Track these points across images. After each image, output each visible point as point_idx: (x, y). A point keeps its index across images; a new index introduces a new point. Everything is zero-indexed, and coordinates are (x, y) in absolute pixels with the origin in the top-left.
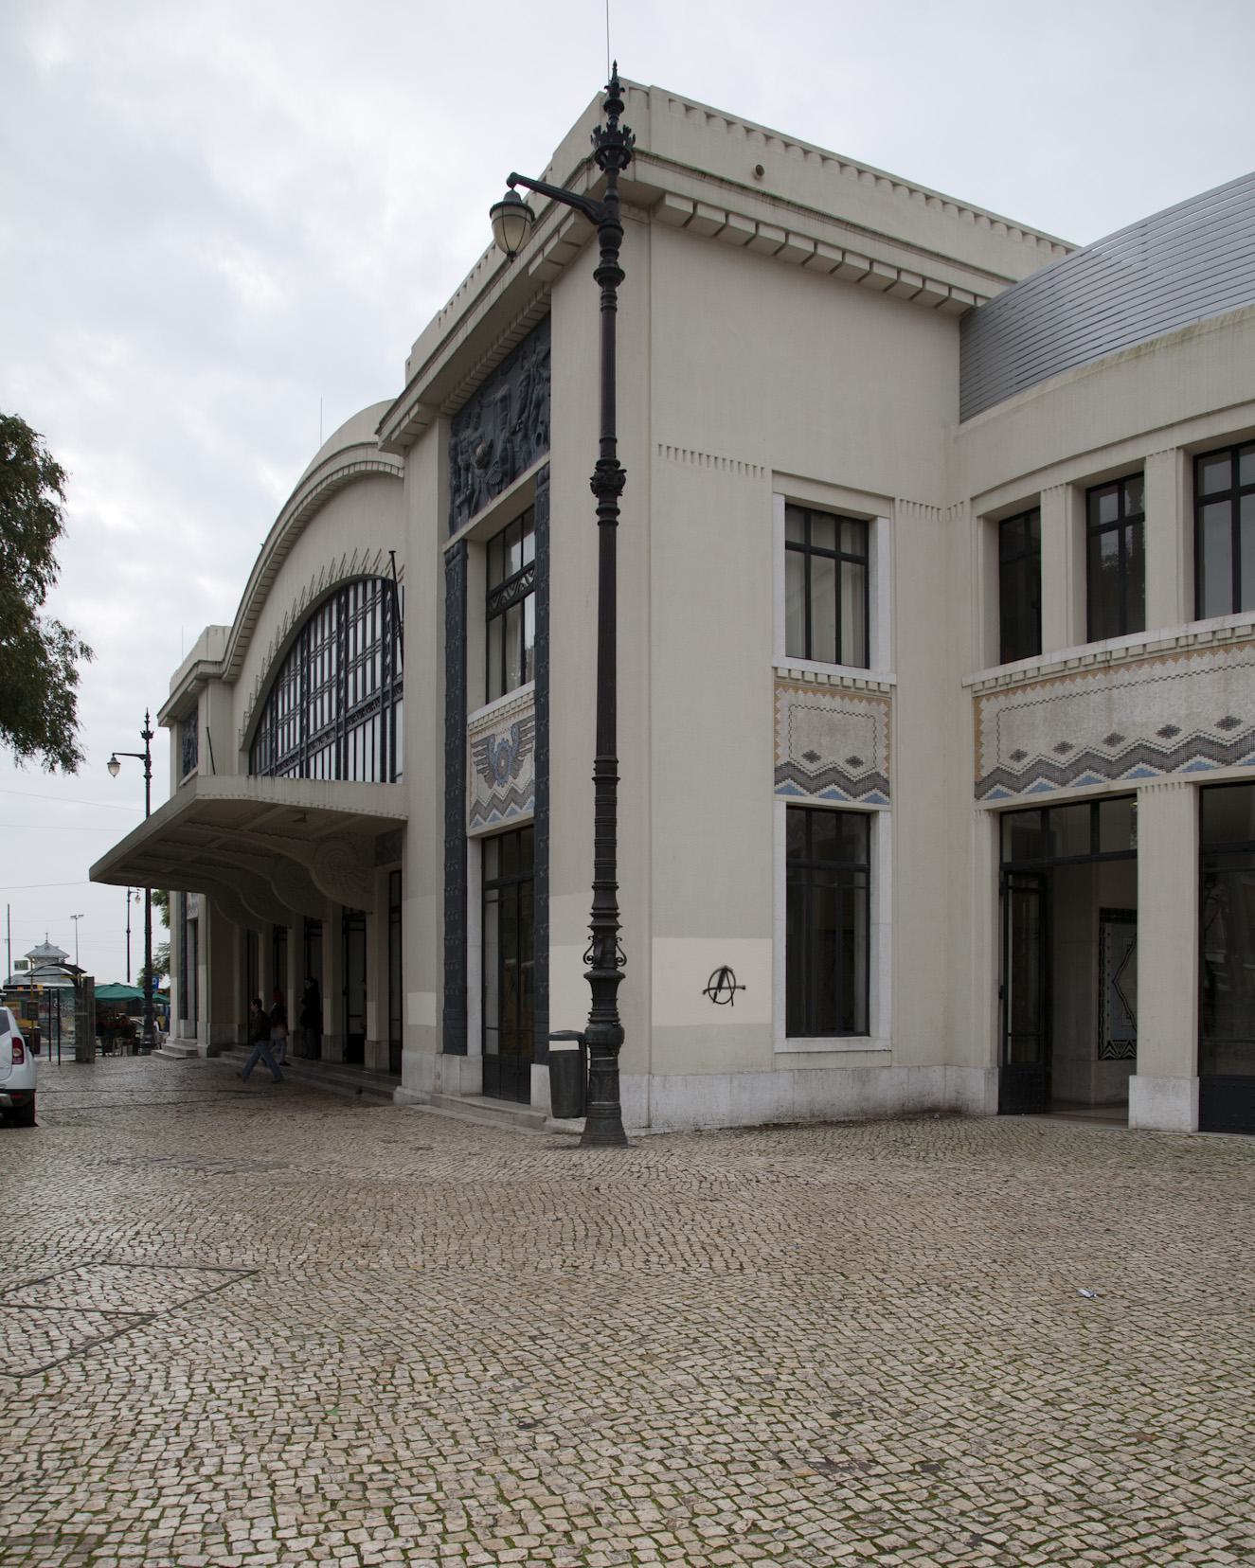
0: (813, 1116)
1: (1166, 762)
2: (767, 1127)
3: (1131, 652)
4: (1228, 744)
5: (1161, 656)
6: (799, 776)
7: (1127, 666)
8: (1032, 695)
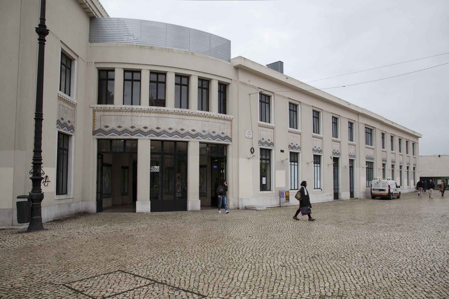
0: (61, 217)
1: (145, 134)
2: (54, 221)
3: (138, 109)
6: (220, 137)
7: (137, 112)
8: (111, 113)
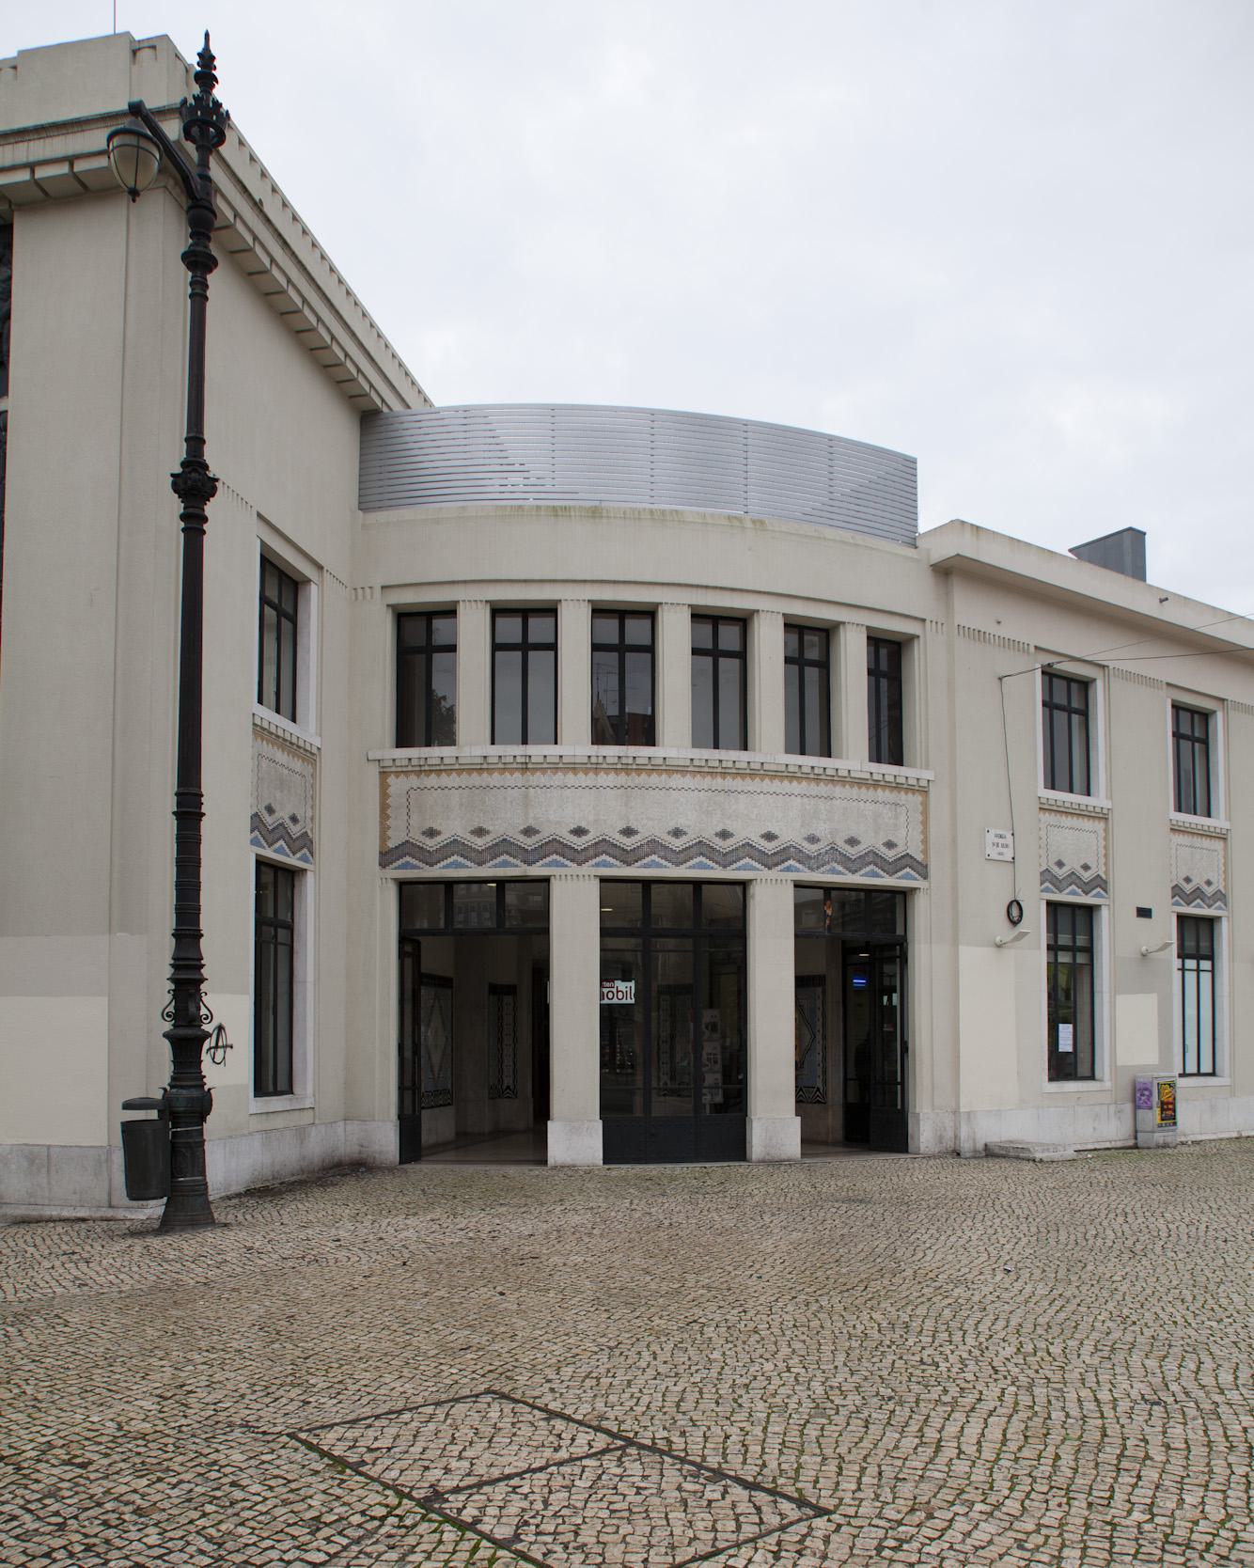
1: (579, 857)
4: (579, 848)
5: (574, 768)
7: (544, 770)
8: (445, 780)
